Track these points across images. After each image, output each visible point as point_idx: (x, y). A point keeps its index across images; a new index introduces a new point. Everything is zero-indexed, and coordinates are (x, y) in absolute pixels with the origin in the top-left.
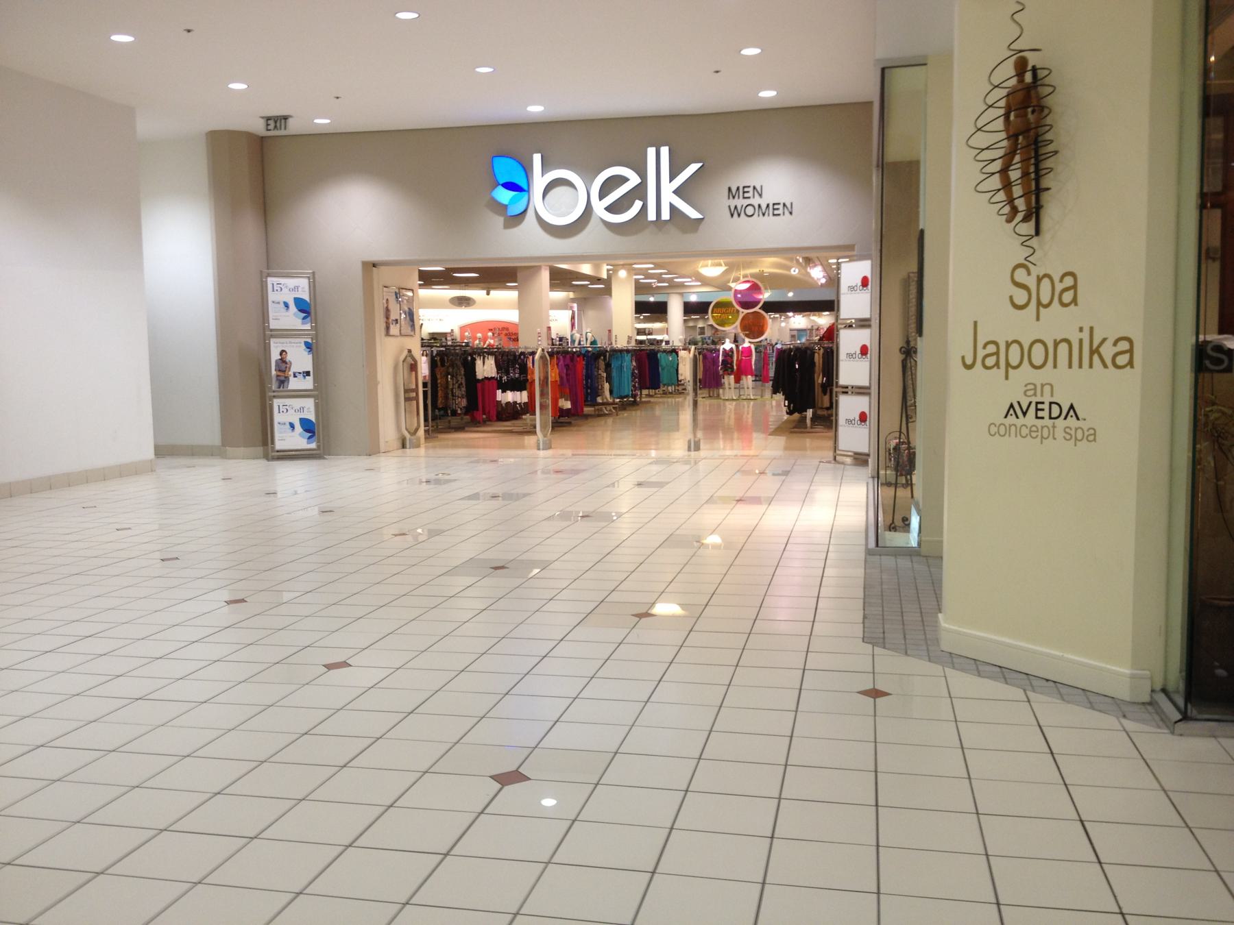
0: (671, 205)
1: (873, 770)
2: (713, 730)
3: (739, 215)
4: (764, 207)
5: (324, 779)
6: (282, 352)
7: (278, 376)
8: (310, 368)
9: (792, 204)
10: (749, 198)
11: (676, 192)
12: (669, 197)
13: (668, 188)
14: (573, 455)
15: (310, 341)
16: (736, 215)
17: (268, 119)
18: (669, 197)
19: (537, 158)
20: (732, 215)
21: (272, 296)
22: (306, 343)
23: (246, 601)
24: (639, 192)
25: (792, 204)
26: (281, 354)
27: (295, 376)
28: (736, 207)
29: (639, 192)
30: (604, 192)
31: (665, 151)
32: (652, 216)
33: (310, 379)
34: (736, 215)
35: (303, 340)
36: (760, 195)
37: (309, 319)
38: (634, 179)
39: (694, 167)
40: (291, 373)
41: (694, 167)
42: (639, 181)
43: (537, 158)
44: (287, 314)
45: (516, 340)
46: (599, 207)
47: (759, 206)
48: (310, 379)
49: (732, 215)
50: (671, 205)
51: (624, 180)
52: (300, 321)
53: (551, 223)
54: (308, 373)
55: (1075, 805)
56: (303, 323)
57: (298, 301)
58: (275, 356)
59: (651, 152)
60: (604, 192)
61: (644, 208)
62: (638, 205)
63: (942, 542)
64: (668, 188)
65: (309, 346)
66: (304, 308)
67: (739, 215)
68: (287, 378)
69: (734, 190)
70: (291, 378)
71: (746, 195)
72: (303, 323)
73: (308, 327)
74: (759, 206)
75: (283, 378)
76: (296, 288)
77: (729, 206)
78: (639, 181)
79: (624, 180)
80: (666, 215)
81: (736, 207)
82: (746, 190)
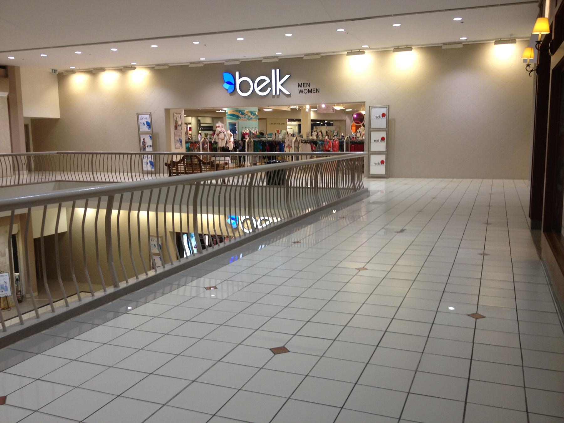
0: (280, 89)
1: (470, 380)
2: (387, 331)
3: (302, 93)
4: (310, 90)
5: (394, 313)
6: (144, 139)
7: (143, 147)
8: (151, 144)
9: (319, 89)
10: (305, 87)
11: (282, 85)
12: (279, 87)
13: (279, 83)
14: (283, 185)
15: (151, 135)
16: (301, 93)
17: (52, 70)
18: (279, 87)
19: (237, 73)
20: (300, 93)
21: (140, 121)
22: (150, 136)
23: (405, 230)
24: (270, 85)
25: (319, 89)
26: (143, 140)
27: (148, 147)
28: (301, 90)
29: (270, 85)
30: (258, 85)
31: (278, 71)
32: (274, 93)
33: (151, 148)
34: (301, 93)
35: (149, 135)
36: (309, 86)
37: (150, 128)
38: (268, 81)
39: (287, 76)
40: (146, 146)
41: (287, 76)
42: (269, 81)
43: (237, 73)
44: (144, 126)
45: (303, 137)
46: (257, 90)
47: (309, 90)
48: (151, 148)
49: (300, 93)
50: (280, 89)
51: (265, 81)
52: (148, 129)
53: (265, 94)
54: (151, 146)
55: (50, 403)
56: (149, 130)
57: (147, 122)
58: (142, 140)
59: (273, 71)
60: (258, 85)
61: (271, 89)
62: (269, 89)
63: (201, 244)
64: (279, 83)
65: (150, 137)
66: (149, 125)
67: (302, 93)
68: (146, 147)
69: (300, 84)
70: (147, 148)
71: (304, 86)
72: (149, 130)
73: (150, 131)
74: (309, 90)
75: (144, 147)
76: (146, 118)
77: (299, 90)
78: (269, 81)
79: (265, 81)
80: (278, 93)
81: (301, 90)
82: (314, 90)
